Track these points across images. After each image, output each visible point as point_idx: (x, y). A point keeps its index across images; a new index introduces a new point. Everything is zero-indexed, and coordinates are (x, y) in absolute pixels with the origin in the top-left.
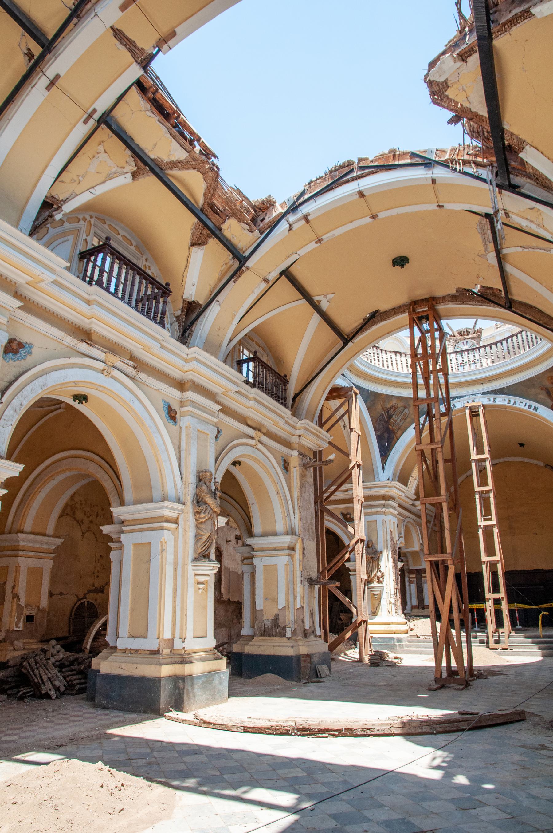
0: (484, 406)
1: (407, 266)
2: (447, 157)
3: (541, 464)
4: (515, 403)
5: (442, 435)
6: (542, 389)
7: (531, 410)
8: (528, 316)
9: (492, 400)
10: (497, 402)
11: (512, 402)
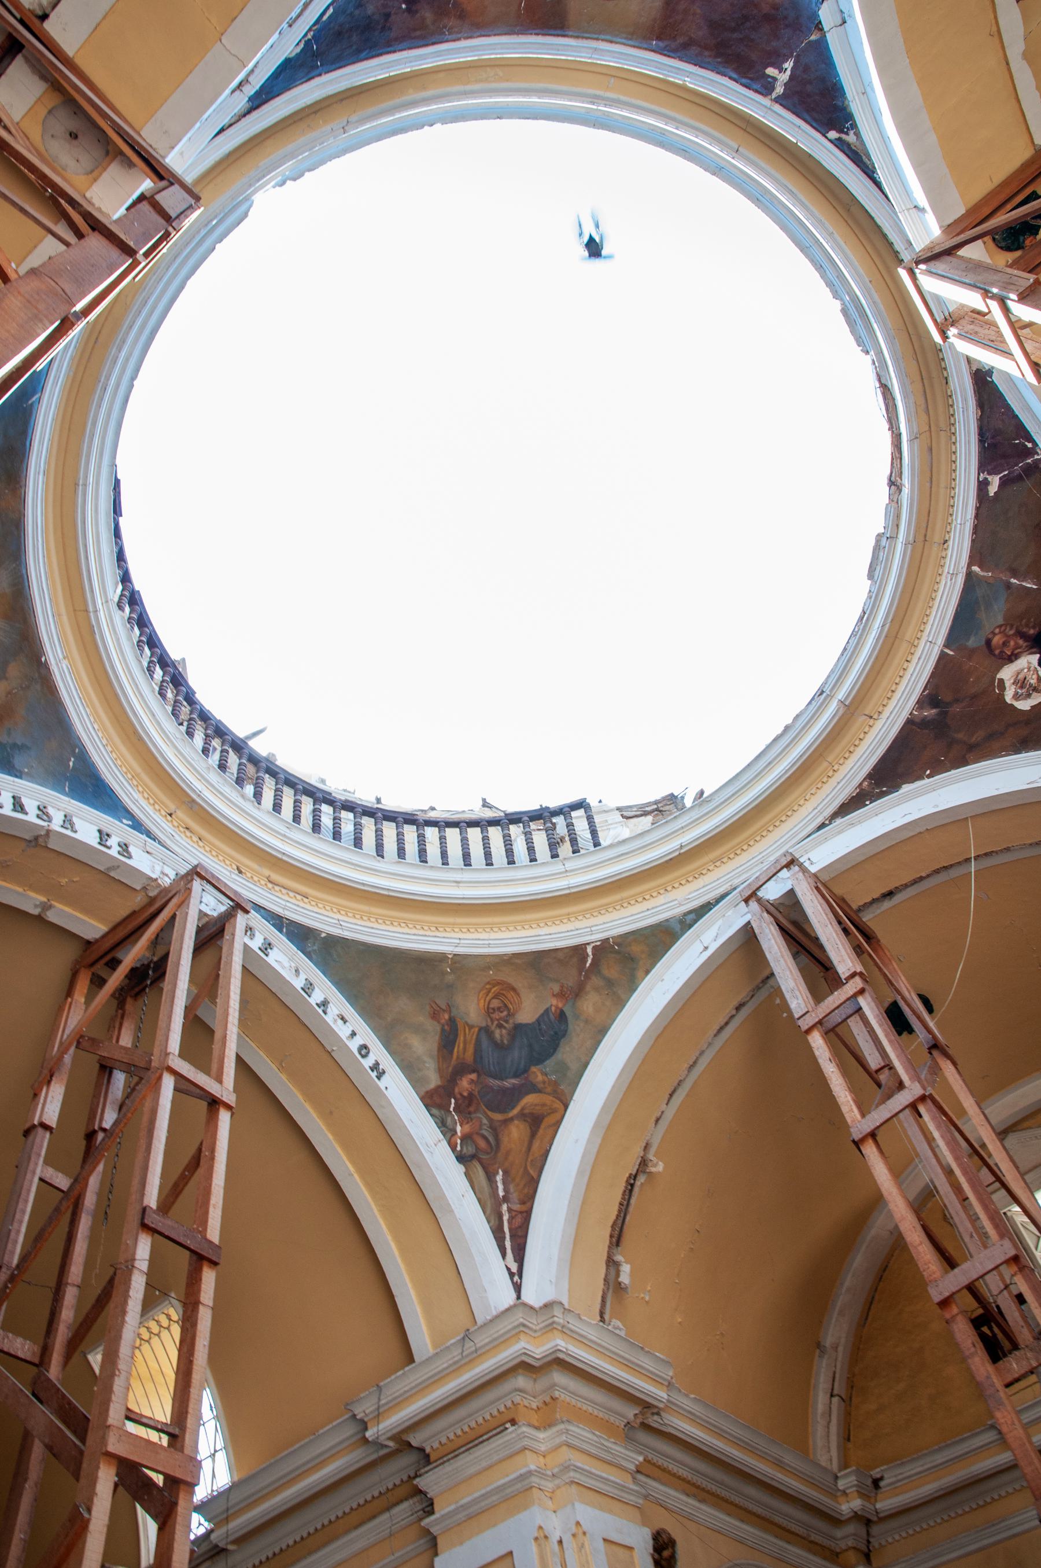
4: (324, 1004)
6: (435, 1016)
11: (317, 997)
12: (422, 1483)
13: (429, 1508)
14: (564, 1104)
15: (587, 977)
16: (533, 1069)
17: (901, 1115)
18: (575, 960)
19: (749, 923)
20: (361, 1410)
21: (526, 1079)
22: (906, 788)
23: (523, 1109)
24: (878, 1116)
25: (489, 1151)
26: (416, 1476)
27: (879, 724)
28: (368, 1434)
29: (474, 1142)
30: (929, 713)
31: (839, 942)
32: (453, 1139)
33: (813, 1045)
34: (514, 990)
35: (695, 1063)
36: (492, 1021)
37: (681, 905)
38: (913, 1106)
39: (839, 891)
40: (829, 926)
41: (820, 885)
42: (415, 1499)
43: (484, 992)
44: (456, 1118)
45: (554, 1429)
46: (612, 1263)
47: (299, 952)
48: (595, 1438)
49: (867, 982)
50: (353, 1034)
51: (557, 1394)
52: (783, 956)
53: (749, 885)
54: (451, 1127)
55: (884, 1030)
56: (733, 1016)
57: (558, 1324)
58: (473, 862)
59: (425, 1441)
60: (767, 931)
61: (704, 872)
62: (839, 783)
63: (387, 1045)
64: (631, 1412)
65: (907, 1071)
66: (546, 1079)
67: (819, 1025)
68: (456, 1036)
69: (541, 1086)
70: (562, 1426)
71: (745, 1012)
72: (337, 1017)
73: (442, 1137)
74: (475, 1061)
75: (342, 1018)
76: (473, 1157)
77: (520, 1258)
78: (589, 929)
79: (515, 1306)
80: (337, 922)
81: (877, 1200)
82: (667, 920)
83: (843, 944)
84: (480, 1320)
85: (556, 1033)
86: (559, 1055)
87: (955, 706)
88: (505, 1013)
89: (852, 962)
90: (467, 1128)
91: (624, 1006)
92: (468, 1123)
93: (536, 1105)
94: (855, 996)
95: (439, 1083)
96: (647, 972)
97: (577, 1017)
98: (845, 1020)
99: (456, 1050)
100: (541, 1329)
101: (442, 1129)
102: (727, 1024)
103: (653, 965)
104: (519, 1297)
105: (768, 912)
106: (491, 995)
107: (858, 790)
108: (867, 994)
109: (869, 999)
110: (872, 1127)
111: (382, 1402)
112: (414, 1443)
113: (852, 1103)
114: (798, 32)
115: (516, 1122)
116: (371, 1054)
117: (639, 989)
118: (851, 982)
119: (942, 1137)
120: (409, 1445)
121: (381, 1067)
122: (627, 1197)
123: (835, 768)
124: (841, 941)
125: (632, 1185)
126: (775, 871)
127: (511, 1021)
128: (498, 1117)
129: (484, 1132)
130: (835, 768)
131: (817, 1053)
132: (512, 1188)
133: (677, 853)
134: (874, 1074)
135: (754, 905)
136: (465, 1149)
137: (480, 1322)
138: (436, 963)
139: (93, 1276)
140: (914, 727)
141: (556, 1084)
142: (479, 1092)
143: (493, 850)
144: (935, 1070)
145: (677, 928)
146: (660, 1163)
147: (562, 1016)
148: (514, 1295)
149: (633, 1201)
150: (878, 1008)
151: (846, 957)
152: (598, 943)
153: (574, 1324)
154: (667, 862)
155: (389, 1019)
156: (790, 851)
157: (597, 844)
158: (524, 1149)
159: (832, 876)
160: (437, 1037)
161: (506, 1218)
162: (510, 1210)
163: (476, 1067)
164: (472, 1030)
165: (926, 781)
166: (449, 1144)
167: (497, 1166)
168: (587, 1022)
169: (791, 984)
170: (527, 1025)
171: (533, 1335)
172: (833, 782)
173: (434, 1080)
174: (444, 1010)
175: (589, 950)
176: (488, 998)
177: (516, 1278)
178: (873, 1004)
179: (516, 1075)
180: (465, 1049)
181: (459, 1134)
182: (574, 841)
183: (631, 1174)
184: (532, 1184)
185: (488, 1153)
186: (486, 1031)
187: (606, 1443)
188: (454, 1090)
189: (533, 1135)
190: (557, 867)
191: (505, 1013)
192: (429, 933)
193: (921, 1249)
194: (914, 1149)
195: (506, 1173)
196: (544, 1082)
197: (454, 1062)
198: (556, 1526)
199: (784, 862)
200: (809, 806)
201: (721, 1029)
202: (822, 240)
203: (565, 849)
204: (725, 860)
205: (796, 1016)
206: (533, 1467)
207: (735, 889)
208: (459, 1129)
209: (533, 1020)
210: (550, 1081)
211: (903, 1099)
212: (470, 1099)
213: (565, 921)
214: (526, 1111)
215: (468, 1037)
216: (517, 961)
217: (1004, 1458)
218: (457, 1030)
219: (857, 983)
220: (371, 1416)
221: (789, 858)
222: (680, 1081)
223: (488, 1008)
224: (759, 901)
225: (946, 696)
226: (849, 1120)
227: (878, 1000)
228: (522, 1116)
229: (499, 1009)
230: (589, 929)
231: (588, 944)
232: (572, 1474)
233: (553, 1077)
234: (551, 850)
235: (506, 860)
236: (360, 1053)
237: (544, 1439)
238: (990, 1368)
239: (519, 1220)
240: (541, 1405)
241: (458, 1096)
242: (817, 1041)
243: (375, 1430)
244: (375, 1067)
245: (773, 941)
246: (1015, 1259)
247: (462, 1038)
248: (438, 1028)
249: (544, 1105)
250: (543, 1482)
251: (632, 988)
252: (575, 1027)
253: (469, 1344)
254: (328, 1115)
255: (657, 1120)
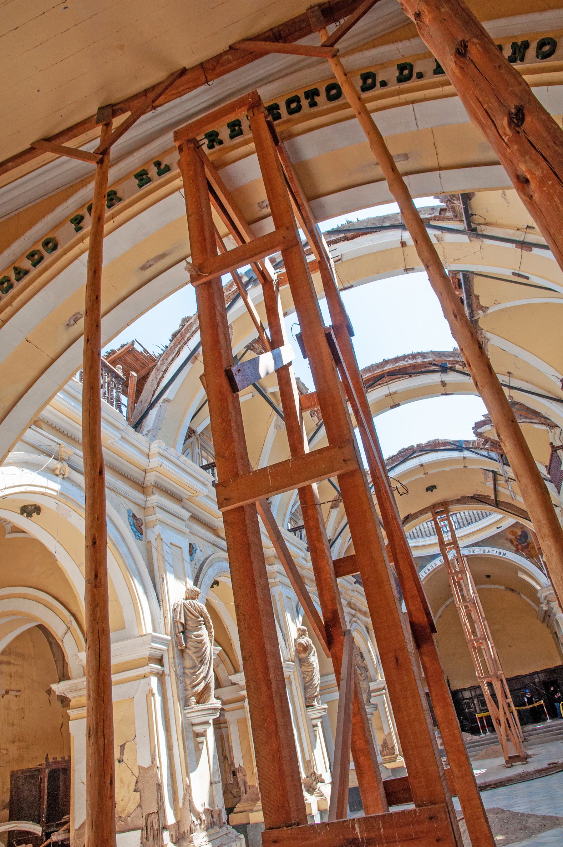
0: (466, 556)
1: (434, 490)
2: (471, 446)
3: (502, 588)
4: (489, 551)
5: (280, 408)
6: (506, 540)
7: (501, 555)
8: (508, 510)
9: (472, 551)
10: (476, 553)
11: (487, 551)
114: (222, 725)
139: (425, 360)
173: (515, 549)
202: (375, 501)
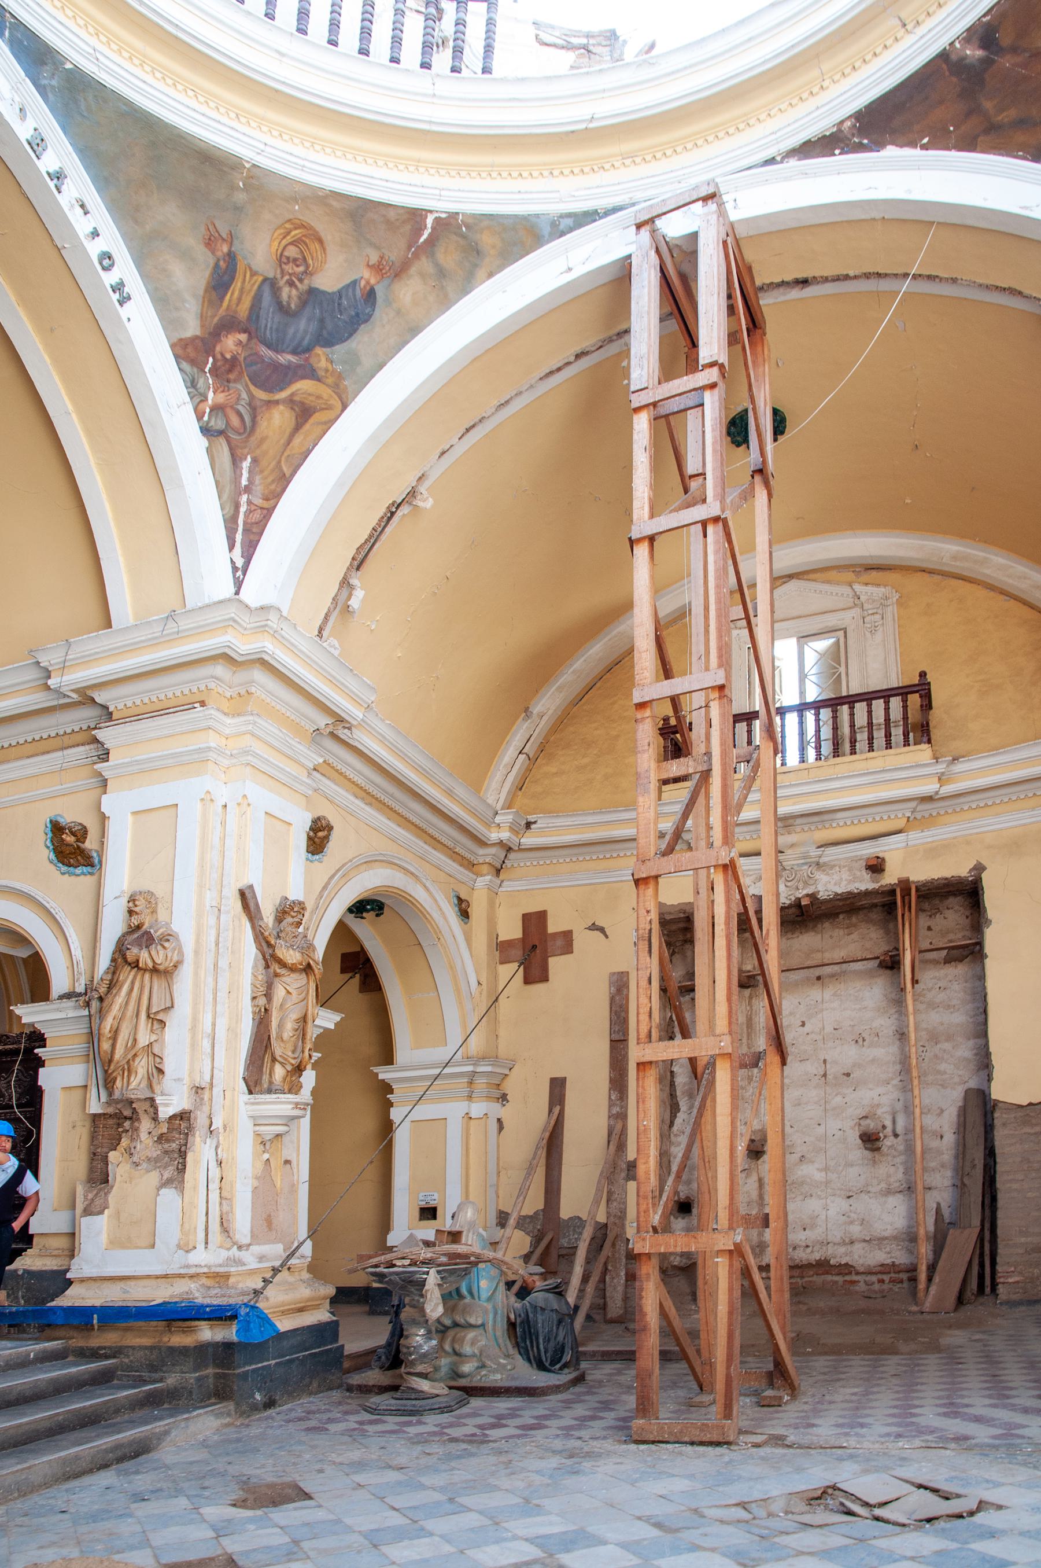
4: (58, 176)
6: (210, 243)
11: (48, 163)
12: (100, 734)
13: (105, 756)
14: (342, 403)
15: (416, 255)
16: (319, 350)
17: (692, 527)
18: (408, 227)
19: (629, 256)
20: (45, 659)
21: (307, 360)
22: (891, 151)
23: (293, 394)
24: (665, 522)
25: (242, 431)
26: (95, 728)
27: (909, 40)
28: (50, 682)
29: (225, 415)
30: (974, 53)
31: (716, 320)
32: (201, 406)
33: (635, 426)
34: (321, 241)
35: (507, 402)
36: (282, 271)
37: (561, 201)
38: (704, 524)
39: (749, 256)
40: (716, 296)
41: (729, 240)
42: (92, 746)
43: (282, 231)
44: (211, 381)
45: (242, 719)
46: (345, 583)
47: (27, 80)
48: (281, 734)
49: (724, 377)
50: (95, 234)
51: (253, 690)
52: (648, 313)
53: (651, 206)
54: (202, 390)
55: (714, 437)
56: (568, 364)
57: (271, 628)
58: (310, 30)
59: (110, 701)
60: (646, 275)
61: (607, 166)
62: (818, 108)
63: (140, 261)
64: (323, 721)
65: (715, 487)
66: (330, 367)
67: (651, 407)
68: (233, 278)
69: (321, 373)
70: (251, 718)
71: (585, 363)
72: (74, 202)
73: (188, 399)
74: (249, 318)
75: (82, 206)
76: (221, 433)
77: (248, 557)
78: (437, 192)
79: (229, 600)
80: (92, 51)
81: (627, 607)
82: (537, 216)
83: (719, 324)
84: (190, 604)
85: (357, 315)
86: (353, 344)
87: (1008, 57)
88: (301, 269)
89: (719, 349)
90: (221, 398)
91: (449, 308)
92: (223, 391)
93: (310, 395)
94: (704, 388)
95: (198, 333)
96: (491, 275)
97: (388, 302)
98: (686, 410)
99: (228, 297)
100: (251, 629)
101: (191, 390)
102: (559, 369)
103: (501, 268)
104: (237, 593)
105: (658, 251)
106: (289, 239)
107: (835, 129)
108: (716, 391)
109: (716, 398)
110: (655, 532)
111: (71, 657)
112: (98, 700)
113: (646, 501)
115: (281, 407)
116: (115, 268)
117: (473, 293)
118: (707, 371)
119: (715, 562)
120: (93, 700)
121: (126, 289)
122: (383, 524)
123: (825, 84)
124: (719, 316)
125: (393, 514)
126: (688, 200)
127: (306, 282)
128: (261, 395)
129: (240, 408)
130: (825, 84)
131: (635, 437)
132: (258, 480)
133: (583, 126)
134: (687, 478)
135: (645, 233)
136: (213, 420)
137: (189, 606)
138: (225, 169)
140: (944, 66)
141: (340, 377)
142: (245, 359)
143: (344, 21)
144: (748, 495)
145: (546, 230)
146: (430, 499)
147: (370, 295)
148: (233, 590)
149: (388, 530)
150: (720, 411)
151: (715, 340)
152: (444, 216)
153: (287, 632)
154: (567, 133)
155: (148, 227)
156: (717, 180)
157: (486, 70)
158: (282, 441)
159: (751, 233)
160: (207, 273)
161: (243, 509)
162: (249, 502)
163: (250, 326)
164: (255, 278)
165: (917, 152)
166: (196, 410)
167: (246, 451)
168: (398, 312)
169: (644, 349)
170: (324, 293)
171: (242, 631)
172: (812, 103)
173: (192, 328)
174: (223, 239)
175: (430, 221)
176: (284, 242)
177: (239, 574)
178: (717, 404)
179: (294, 352)
180: (239, 300)
181: (210, 402)
182: (458, 52)
183: (394, 502)
184: (284, 481)
185: (240, 434)
186: (272, 283)
187: (290, 741)
188: (214, 347)
189: (298, 428)
190: (423, 81)
191: (301, 269)
192: (224, 119)
193: (644, 655)
194: (689, 566)
195: (255, 461)
196: (327, 371)
197: (222, 312)
198: (223, 793)
199: (704, 192)
200: (771, 125)
201: (551, 373)
203: (442, 59)
204: (638, 160)
205: (633, 388)
206: (213, 745)
207: (633, 204)
208: (211, 395)
209: (335, 289)
210: (334, 371)
211: (699, 513)
212: (232, 364)
213: (411, 169)
214: (297, 398)
215: (247, 286)
216: (335, 204)
217: (629, 832)
218: (235, 271)
219: (712, 375)
220: (57, 667)
221: (711, 190)
222: (483, 418)
223: (281, 255)
224: (654, 232)
225: (1005, 39)
226: (635, 517)
227: (726, 402)
228: (290, 401)
229: (295, 260)
230: (437, 192)
231: (431, 212)
232: (249, 758)
233: (339, 368)
234: (423, 54)
235: (357, 45)
236: (101, 263)
237: (230, 724)
238: (653, 765)
239: (257, 516)
240: (235, 695)
241: (219, 356)
242: (642, 424)
243: (59, 680)
244: (118, 287)
245: (646, 290)
246: (721, 688)
247: (239, 285)
248: (212, 262)
249: (319, 397)
250: (220, 758)
251: (465, 290)
252: (382, 314)
253: (171, 624)
254: (47, 330)
255: (443, 453)
